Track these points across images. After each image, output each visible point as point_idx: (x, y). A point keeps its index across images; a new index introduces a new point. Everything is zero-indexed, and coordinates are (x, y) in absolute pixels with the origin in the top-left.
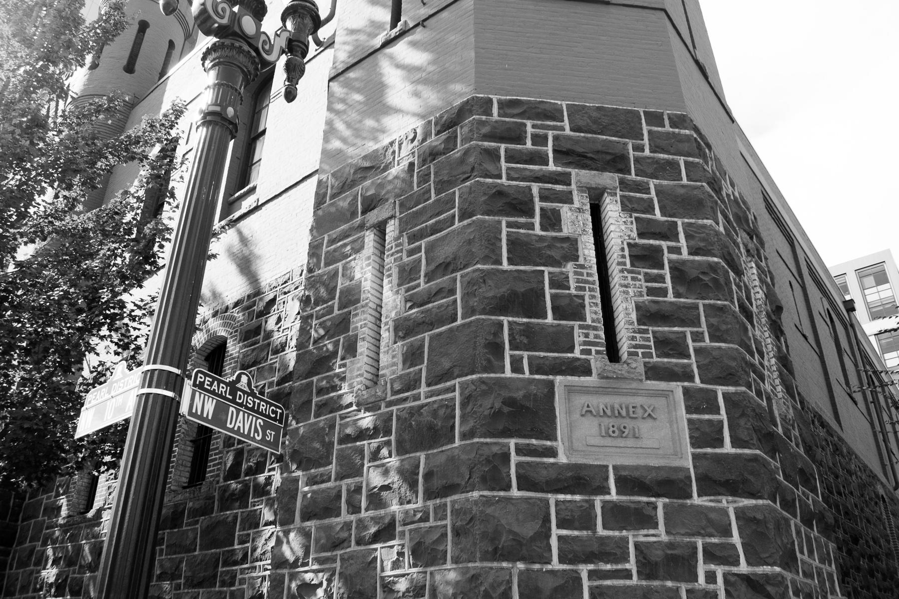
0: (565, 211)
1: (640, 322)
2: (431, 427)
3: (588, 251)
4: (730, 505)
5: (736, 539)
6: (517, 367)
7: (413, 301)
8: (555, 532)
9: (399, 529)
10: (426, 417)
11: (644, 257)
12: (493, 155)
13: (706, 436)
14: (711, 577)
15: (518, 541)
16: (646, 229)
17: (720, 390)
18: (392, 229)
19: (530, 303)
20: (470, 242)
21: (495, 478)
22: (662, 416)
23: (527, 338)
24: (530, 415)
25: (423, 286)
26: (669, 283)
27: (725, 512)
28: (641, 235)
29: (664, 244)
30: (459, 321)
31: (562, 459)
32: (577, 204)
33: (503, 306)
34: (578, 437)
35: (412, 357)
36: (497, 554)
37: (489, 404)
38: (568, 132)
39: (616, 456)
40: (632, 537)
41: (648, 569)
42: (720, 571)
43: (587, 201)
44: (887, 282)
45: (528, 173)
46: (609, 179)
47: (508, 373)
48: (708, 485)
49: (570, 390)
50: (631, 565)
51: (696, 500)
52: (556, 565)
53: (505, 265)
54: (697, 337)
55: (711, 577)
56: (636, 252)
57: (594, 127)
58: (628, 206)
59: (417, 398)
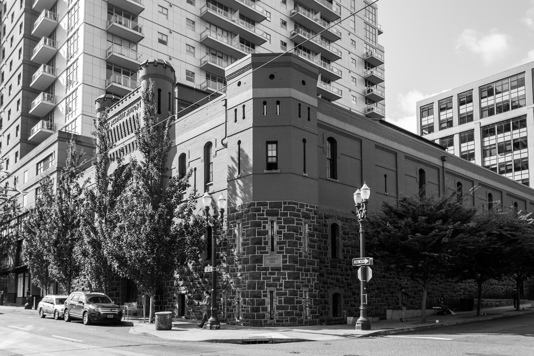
0: (267, 226)
4: (286, 272)
6: (258, 253)
7: (244, 240)
11: (279, 233)
13: (285, 262)
16: (280, 227)
23: (259, 248)
34: (266, 262)
35: (244, 249)
41: (274, 280)
46: (275, 218)
49: (265, 256)
58: (278, 223)
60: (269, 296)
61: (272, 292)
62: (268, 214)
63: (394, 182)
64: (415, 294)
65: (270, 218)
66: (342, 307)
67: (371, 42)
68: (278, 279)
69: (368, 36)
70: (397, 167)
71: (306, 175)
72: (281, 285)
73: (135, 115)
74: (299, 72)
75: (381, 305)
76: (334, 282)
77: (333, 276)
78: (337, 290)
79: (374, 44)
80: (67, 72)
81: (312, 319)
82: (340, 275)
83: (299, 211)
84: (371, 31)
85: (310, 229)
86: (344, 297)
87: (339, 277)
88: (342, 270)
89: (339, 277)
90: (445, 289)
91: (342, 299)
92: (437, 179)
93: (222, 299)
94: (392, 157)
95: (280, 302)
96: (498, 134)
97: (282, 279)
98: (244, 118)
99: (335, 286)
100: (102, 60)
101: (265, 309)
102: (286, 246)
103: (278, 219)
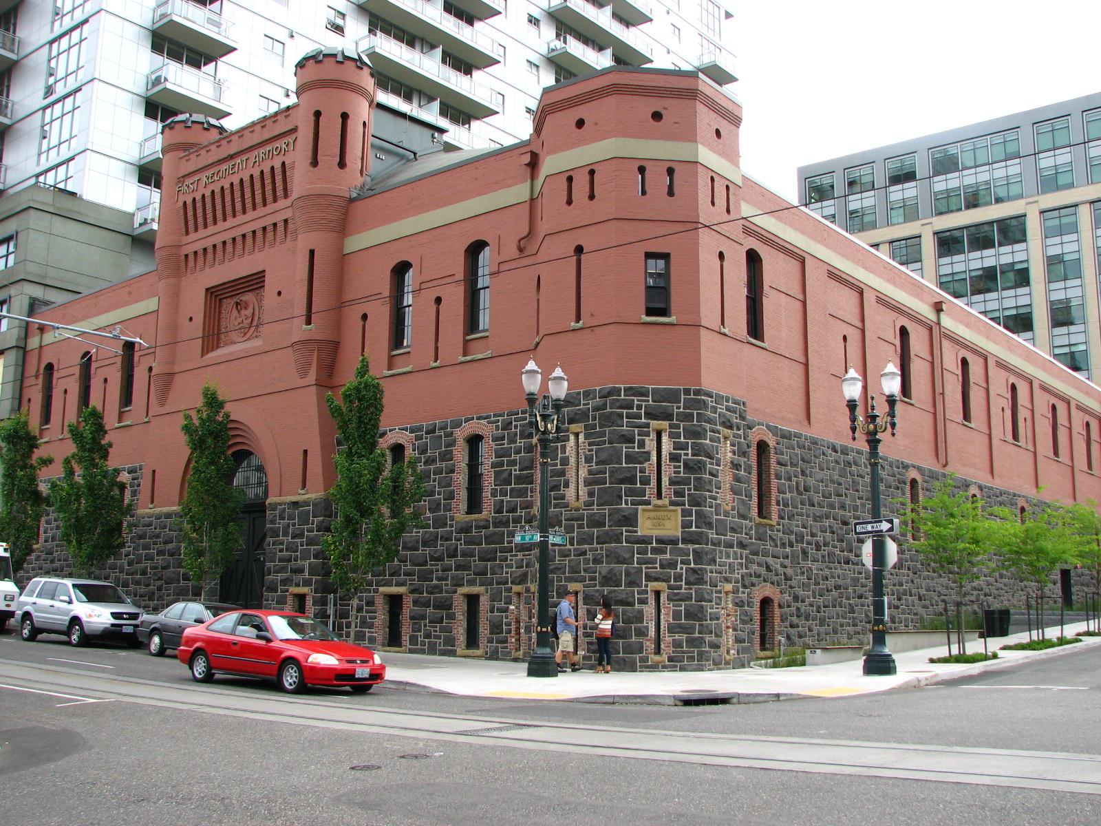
0: (647, 442)
1: (669, 485)
2: (598, 521)
3: (654, 458)
4: (691, 547)
5: (691, 557)
6: (626, 504)
7: (590, 472)
8: (636, 555)
9: (588, 553)
10: (597, 518)
11: (674, 458)
12: (621, 416)
13: (686, 525)
14: (682, 569)
15: (625, 559)
16: (677, 446)
17: (694, 508)
18: (581, 437)
19: (631, 480)
20: (612, 455)
21: (618, 540)
22: (672, 518)
23: (630, 493)
24: (631, 520)
25: (594, 467)
26: (682, 469)
27: (689, 549)
28: (674, 449)
29: (682, 452)
30: (608, 485)
31: (639, 534)
32: (651, 437)
33: (622, 481)
34: (645, 527)
35: (591, 494)
36: (618, 563)
37: (616, 517)
38: (651, 403)
39: (656, 533)
40: (659, 557)
41: (662, 566)
42: (684, 567)
43: (655, 436)
44: (1025, 241)
45: (633, 424)
46: (665, 424)
47: (624, 506)
48: (685, 541)
49: (644, 510)
50: (658, 565)
51: (680, 545)
52: (636, 565)
53: (624, 465)
54: (689, 489)
55: (682, 569)
56: (672, 457)
57: (661, 400)
58: (671, 436)
59: (593, 510)
60: (652, 601)
61: (658, 594)
62: (649, 415)
63: (859, 352)
64: (899, 599)
65: (655, 424)
66: (776, 628)
67: (710, 35)
68: (673, 565)
69: (705, 21)
70: (863, 320)
71: (726, 331)
72: (678, 577)
73: (278, 166)
74: (711, 112)
75: (842, 625)
76: (763, 571)
77: (760, 558)
78: (768, 590)
79: (716, 39)
80: (50, 50)
81: (738, 654)
82: (774, 557)
83: (714, 410)
84: (711, 10)
85: (734, 453)
86: (780, 606)
87: (770, 560)
88: (776, 546)
89: (770, 560)
90: (947, 588)
91: (777, 610)
92: (927, 348)
93: (512, 607)
94: (850, 298)
95: (677, 615)
96: (969, 252)
97: (682, 563)
98: (592, 197)
99: (765, 581)
100: (142, 30)
101: (642, 633)
102: (689, 489)
103: (671, 426)
